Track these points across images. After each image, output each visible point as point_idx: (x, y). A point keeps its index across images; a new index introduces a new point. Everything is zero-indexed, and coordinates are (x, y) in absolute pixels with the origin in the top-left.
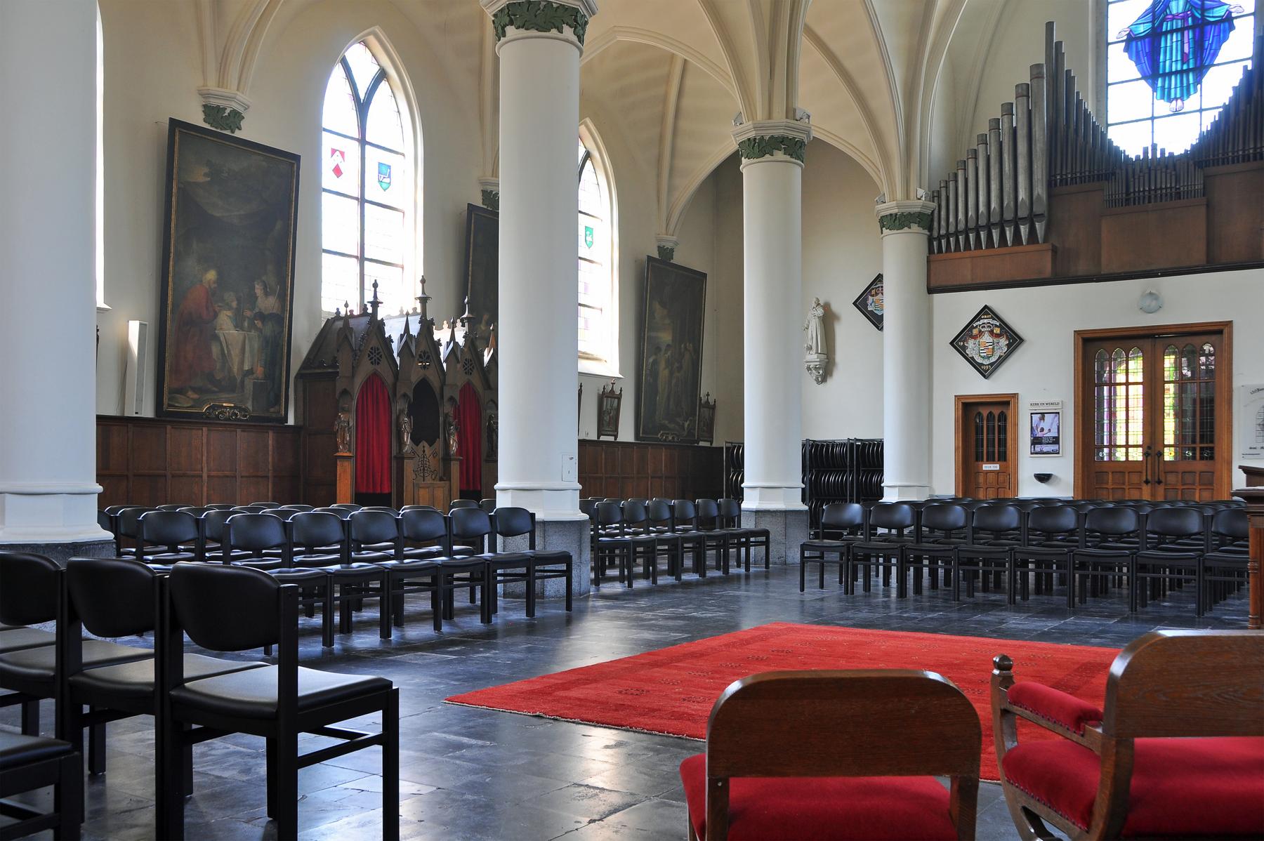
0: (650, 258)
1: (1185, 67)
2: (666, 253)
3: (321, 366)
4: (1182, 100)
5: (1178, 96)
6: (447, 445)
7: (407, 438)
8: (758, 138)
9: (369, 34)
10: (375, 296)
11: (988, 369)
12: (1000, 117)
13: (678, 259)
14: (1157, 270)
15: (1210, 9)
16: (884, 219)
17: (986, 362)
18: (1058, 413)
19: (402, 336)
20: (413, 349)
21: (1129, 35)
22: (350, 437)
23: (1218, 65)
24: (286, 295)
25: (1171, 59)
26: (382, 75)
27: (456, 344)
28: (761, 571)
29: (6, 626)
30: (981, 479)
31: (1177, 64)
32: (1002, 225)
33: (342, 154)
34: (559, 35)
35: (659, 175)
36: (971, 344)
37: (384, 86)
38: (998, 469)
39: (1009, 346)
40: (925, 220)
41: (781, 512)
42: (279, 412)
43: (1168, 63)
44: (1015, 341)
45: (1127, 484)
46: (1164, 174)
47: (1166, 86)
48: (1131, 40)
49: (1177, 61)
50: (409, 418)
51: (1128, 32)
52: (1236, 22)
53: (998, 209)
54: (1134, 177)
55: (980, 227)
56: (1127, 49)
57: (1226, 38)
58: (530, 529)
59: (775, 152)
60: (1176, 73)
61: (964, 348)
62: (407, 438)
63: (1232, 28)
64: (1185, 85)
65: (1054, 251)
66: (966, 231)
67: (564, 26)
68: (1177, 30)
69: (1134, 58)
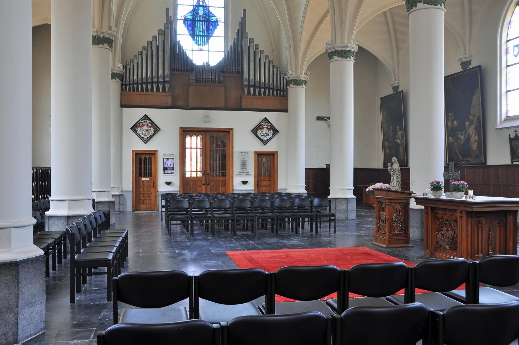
4: (203, 46)
5: (201, 44)
8: (97, 36)
11: (146, 140)
14: (209, 108)
15: (211, 16)
17: (145, 137)
18: (174, 158)
21: (185, 18)
23: (214, 36)
29: (265, 306)
30: (141, 184)
31: (201, 33)
38: (148, 180)
39: (154, 131)
41: (107, 202)
43: (198, 31)
44: (157, 129)
46: (211, 73)
48: (185, 20)
49: (201, 32)
51: (184, 17)
52: (219, 23)
54: (202, 72)
55: (139, 83)
56: (184, 23)
57: (216, 28)
59: (105, 44)
60: (201, 36)
61: (136, 131)
63: (218, 25)
64: (204, 41)
66: (137, 84)
68: (201, 21)
69: (187, 27)
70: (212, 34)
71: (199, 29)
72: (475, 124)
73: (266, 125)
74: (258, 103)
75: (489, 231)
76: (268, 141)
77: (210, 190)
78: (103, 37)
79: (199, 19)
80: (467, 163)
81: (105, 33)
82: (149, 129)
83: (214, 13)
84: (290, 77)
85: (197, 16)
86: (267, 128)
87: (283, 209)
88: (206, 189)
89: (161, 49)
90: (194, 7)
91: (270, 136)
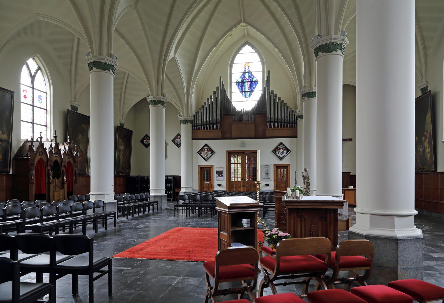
0: (118, 126)
1: (249, 91)
2: (122, 125)
3: (22, 156)
5: (247, 97)
6: (63, 179)
7: (51, 177)
9: (35, 56)
10: (41, 136)
12: (209, 98)
13: (125, 127)
16: (181, 121)
17: (206, 157)
19: (49, 148)
20: (53, 151)
21: (237, 81)
22: (33, 177)
24: (10, 134)
25: (246, 88)
26: (39, 69)
27: (66, 150)
28: (156, 212)
30: (205, 186)
32: (210, 124)
33: (27, 91)
34: (109, 72)
35: (120, 104)
36: (202, 153)
37: (39, 72)
38: (209, 183)
39: (211, 154)
40: (191, 122)
42: (7, 170)
43: (245, 89)
44: (213, 152)
45: (238, 186)
47: (245, 94)
50: (52, 172)
52: (258, 82)
53: (209, 121)
56: (236, 85)
58: (103, 206)
60: (247, 92)
61: (201, 154)
62: (51, 177)
63: (258, 83)
65: (222, 131)
66: (201, 125)
67: (110, 69)
68: (247, 82)
70: (254, 90)
71: (246, 87)
72: (428, 138)
73: (282, 147)
74: (277, 133)
75: (311, 224)
76: (283, 157)
77: (246, 190)
78: (158, 100)
79: (246, 81)
80: (424, 170)
81: (307, 90)
82: (208, 152)
83: (255, 76)
84: (298, 114)
85: (244, 79)
86: (283, 149)
87: (197, 201)
88: (244, 189)
89: (214, 103)
90: (243, 73)
91: (285, 154)
